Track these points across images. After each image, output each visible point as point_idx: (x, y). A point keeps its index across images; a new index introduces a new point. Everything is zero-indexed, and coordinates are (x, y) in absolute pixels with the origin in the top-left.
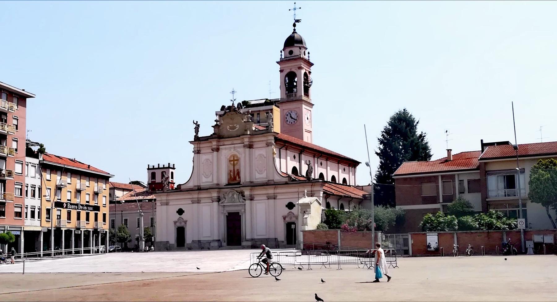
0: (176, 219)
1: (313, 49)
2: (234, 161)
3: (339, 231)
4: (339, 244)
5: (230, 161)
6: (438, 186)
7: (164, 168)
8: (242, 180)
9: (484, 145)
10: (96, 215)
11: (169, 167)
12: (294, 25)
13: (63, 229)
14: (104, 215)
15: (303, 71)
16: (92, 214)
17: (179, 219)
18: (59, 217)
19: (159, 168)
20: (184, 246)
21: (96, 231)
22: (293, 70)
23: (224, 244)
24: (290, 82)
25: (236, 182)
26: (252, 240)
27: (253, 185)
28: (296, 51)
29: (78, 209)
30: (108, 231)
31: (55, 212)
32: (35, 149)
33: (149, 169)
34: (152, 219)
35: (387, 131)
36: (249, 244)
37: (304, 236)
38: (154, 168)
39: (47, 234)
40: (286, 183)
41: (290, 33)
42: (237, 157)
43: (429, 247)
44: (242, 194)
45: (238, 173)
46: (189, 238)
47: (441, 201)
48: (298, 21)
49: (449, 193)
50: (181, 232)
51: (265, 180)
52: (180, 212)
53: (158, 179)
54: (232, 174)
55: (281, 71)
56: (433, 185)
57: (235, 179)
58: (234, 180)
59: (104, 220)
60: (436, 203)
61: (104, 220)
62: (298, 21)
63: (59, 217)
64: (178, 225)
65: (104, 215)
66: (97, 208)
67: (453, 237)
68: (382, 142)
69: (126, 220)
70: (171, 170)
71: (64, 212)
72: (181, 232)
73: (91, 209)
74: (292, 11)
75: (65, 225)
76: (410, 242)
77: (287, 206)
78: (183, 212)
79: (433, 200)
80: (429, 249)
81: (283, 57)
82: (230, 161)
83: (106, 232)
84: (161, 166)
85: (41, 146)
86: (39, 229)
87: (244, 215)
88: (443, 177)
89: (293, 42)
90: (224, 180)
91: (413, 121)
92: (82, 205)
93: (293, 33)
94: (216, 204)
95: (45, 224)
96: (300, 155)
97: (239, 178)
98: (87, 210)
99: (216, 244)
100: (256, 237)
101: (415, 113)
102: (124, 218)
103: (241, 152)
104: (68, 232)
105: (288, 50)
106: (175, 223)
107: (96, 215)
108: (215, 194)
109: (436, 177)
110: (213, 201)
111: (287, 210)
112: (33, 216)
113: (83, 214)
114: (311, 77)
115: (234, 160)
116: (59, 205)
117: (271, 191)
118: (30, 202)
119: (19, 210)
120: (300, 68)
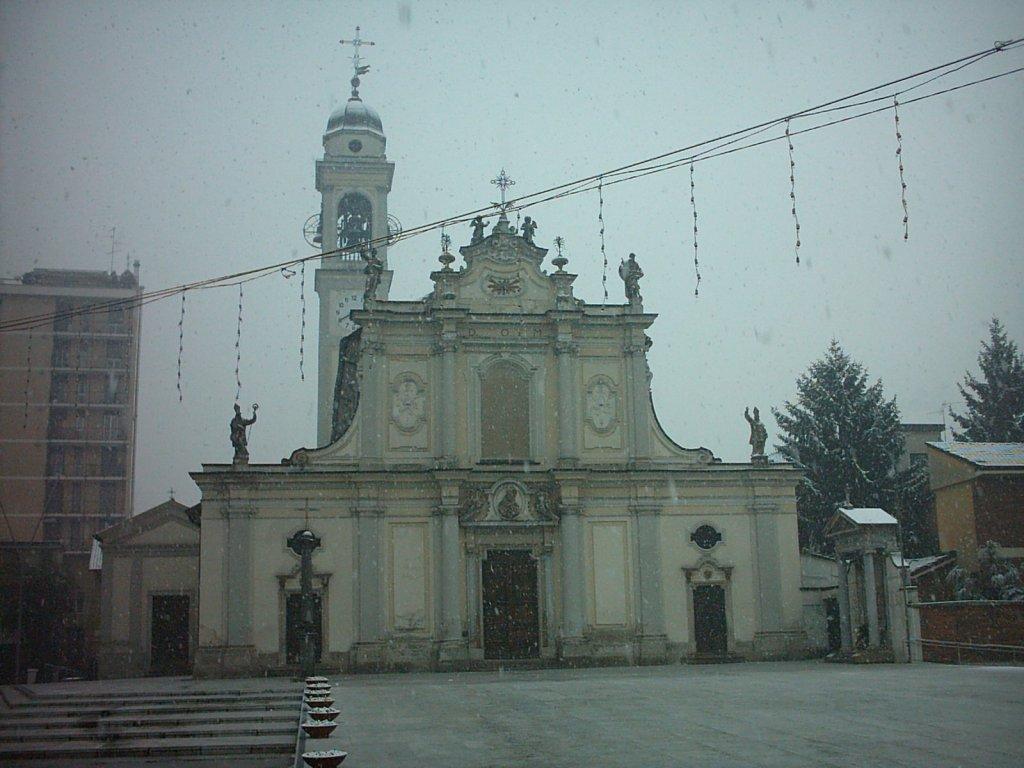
22: (362, 190)
77: (694, 537)
106: (688, 573)
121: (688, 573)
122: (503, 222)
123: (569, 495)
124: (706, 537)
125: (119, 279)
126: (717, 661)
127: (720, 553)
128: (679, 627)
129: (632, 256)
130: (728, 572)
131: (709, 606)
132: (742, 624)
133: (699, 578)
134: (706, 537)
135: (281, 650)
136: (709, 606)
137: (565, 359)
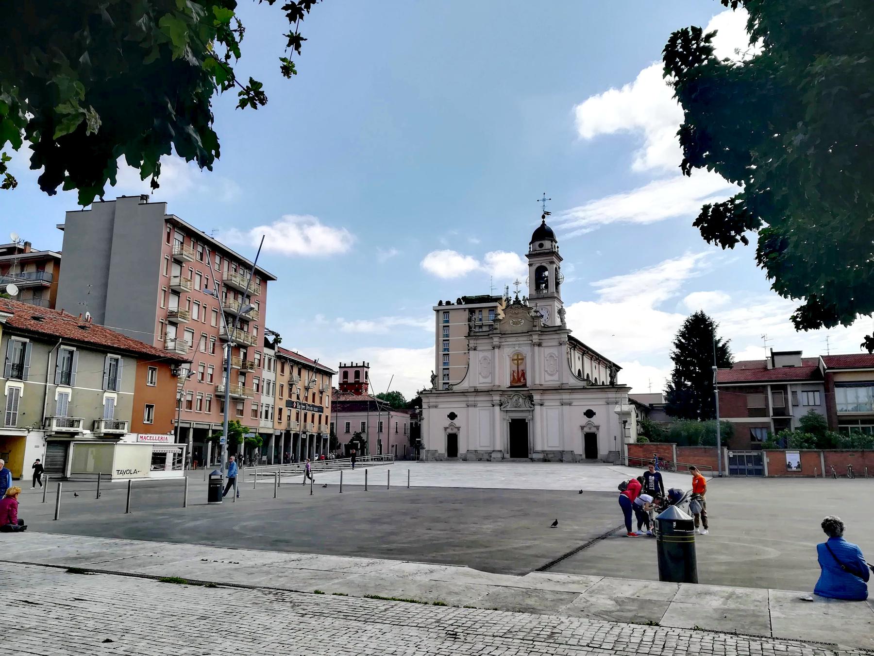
0: (583, 424)
1: (563, 243)
2: (518, 359)
3: (674, 446)
4: (675, 461)
5: (513, 360)
6: (767, 399)
7: (357, 367)
8: (529, 383)
9: (774, 354)
10: (320, 416)
11: (364, 366)
12: (543, 217)
13: (292, 432)
15: (555, 266)
16: (317, 415)
17: (451, 425)
19: (352, 367)
20: (596, 457)
22: (544, 264)
23: (508, 456)
24: (539, 278)
25: (521, 384)
26: (543, 452)
27: (545, 391)
28: (547, 244)
30: (329, 437)
31: (286, 412)
32: (271, 339)
33: (340, 367)
36: (541, 456)
37: (629, 449)
38: (345, 367)
39: (278, 438)
40: (584, 388)
41: (538, 224)
42: (522, 355)
43: (789, 466)
44: (531, 398)
45: (524, 374)
46: (462, 449)
47: (771, 414)
48: (548, 213)
49: (781, 405)
50: (452, 440)
51: (556, 384)
52: (452, 416)
53: (351, 379)
54: (515, 375)
55: (530, 265)
56: (761, 396)
57: (519, 380)
58: (519, 380)
60: (765, 416)
62: (548, 213)
64: (449, 431)
65: (327, 417)
67: (820, 456)
70: (366, 369)
71: (294, 411)
72: (452, 440)
73: (316, 409)
74: (541, 203)
75: (295, 428)
76: (766, 460)
77: (585, 414)
78: (456, 416)
79: (763, 412)
80: (789, 470)
82: (513, 360)
84: (354, 365)
85: (277, 335)
86: (270, 431)
88: (773, 387)
89: (543, 234)
90: (505, 381)
91: (711, 324)
94: (497, 408)
95: (277, 426)
96: (583, 355)
97: (525, 379)
99: (499, 455)
100: (546, 449)
101: (712, 315)
103: (526, 350)
104: (296, 436)
105: (537, 243)
106: (582, 428)
107: (320, 416)
108: (497, 398)
109: (765, 387)
110: (493, 406)
111: (586, 419)
112: (266, 417)
114: (562, 273)
115: (518, 360)
116: (290, 404)
117: (566, 397)
118: (266, 400)
119: (255, 408)
120: (552, 263)
121: (582, 428)
122: (517, 298)
123: (537, 397)
124: (590, 414)
125: (803, 302)
126: (594, 462)
127: (594, 419)
128: (579, 447)
129: (832, 528)
130: (598, 427)
131: (591, 440)
132: (603, 448)
133: (586, 430)
134: (590, 414)
135: (369, 396)
136: (591, 440)
137: (536, 348)
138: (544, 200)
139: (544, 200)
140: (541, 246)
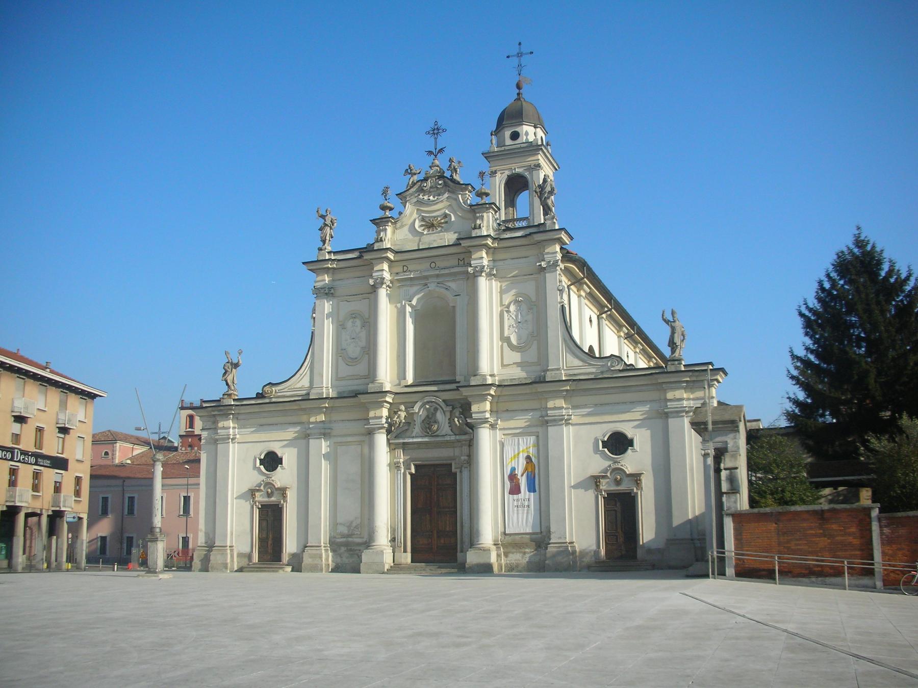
14: (78, 480)
18: (57, 489)
21: (56, 516)
29: (12, 459)
34: (187, 499)
35: (826, 296)
59: (78, 493)
61: (78, 493)
63: (57, 489)
65: (78, 480)
66: (60, 464)
68: (810, 326)
69: (131, 499)
73: (47, 463)
81: (410, 379)
83: (80, 519)
87: (465, 473)
92: (24, 453)
93: (518, 99)
98: (36, 464)
102: (127, 495)
113: (26, 472)
127: (630, 462)
138: (520, 55)
139: (520, 55)
140: (515, 136)
